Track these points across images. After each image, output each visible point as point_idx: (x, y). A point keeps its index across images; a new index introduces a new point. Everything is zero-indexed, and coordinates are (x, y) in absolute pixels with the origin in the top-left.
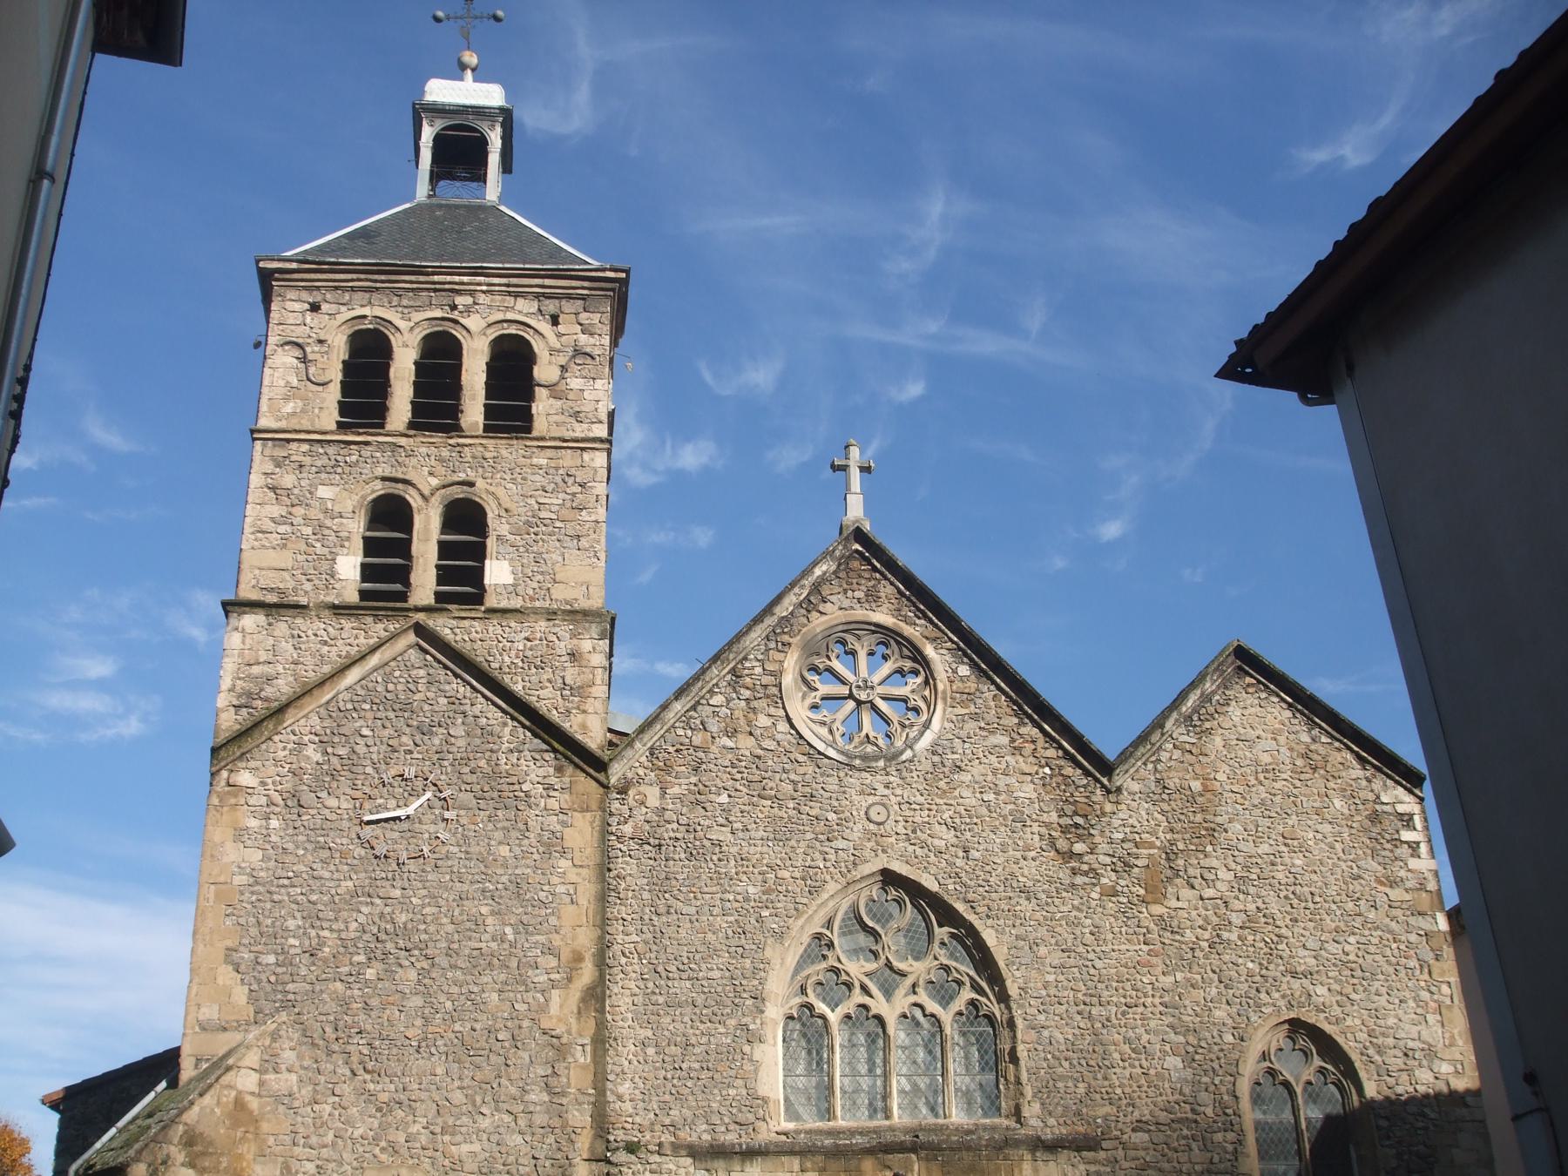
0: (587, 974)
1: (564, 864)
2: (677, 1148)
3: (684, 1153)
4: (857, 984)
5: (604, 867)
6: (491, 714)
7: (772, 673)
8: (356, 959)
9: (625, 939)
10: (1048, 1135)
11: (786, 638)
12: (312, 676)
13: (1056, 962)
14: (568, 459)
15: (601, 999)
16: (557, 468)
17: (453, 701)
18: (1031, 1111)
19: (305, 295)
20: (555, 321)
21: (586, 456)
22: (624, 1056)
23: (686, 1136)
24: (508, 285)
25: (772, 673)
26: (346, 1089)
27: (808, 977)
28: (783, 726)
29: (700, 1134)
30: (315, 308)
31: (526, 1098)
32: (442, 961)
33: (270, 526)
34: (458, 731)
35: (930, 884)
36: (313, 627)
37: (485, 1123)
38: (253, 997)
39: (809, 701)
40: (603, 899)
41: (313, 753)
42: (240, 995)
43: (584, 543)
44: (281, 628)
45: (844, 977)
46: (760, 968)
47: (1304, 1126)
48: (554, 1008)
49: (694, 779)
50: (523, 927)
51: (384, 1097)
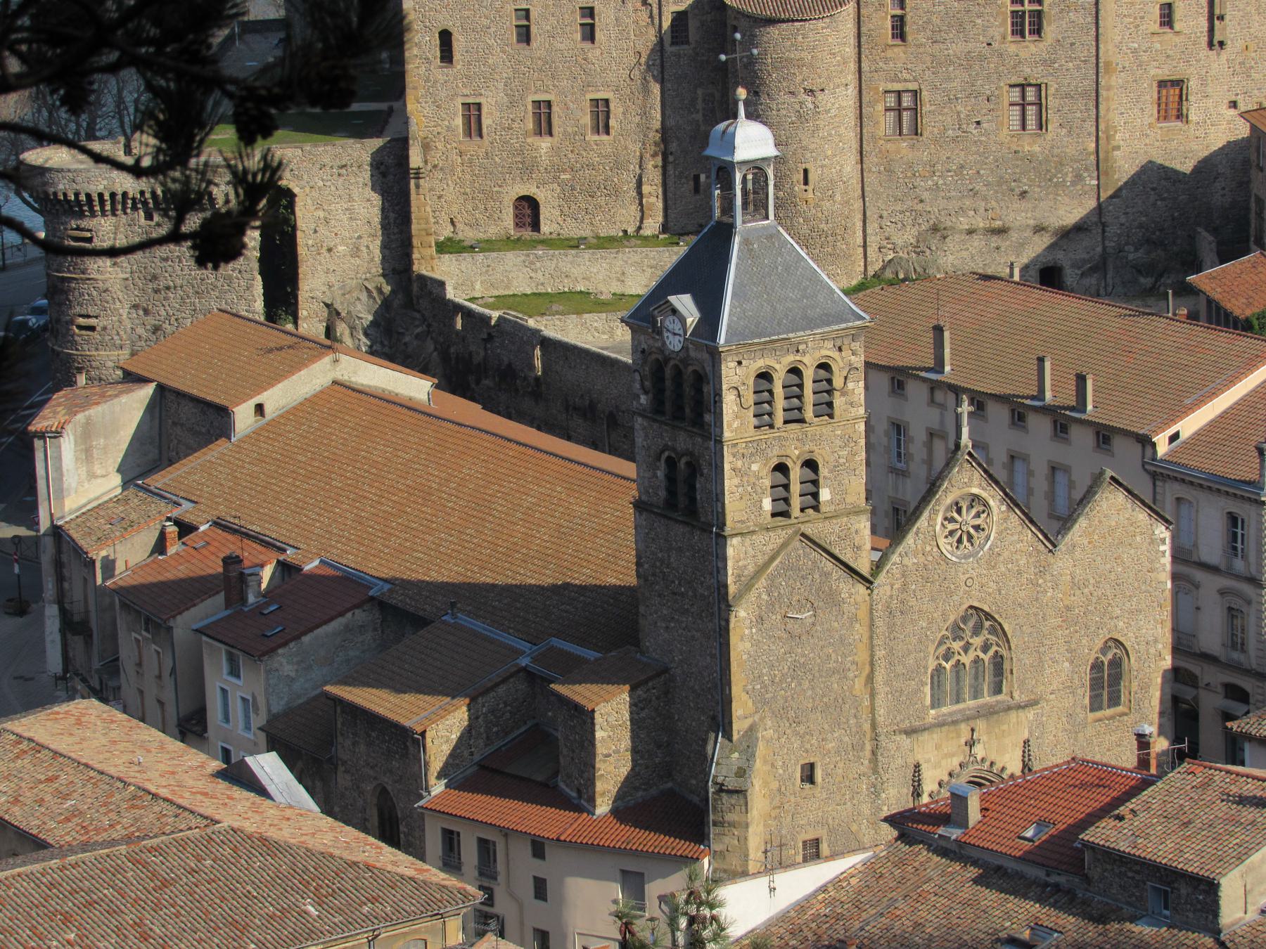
1: (858, 626)
2: (900, 732)
6: (829, 565)
12: (761, 562)
17: (814, 562)
18: (1016, 695)
20: (840, 349)
23: (902, 726)
26: (788, 731)
28: (935, 549)
29: (906, 725)
32: (817, 675)
34: (816, 576)
35: (986, 608)
36: (759, 538)
37: (836, 735)
38: (754, 702)
40: (871, 638)
41: (765, 597)
42: (750, 703)
47: (1039, 873)
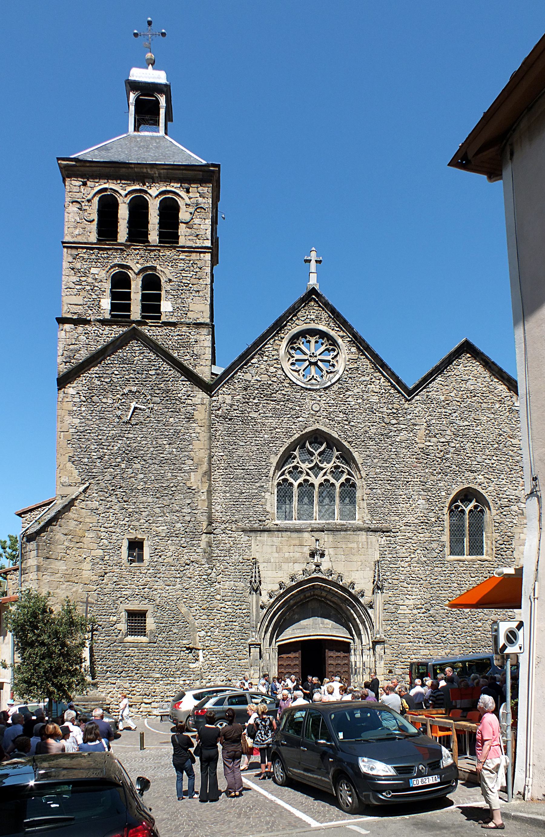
0: (205, 467)
5: (211, 426)
8: (117, 460)
10: (372, 526)
11: (282, 335)
22: (218, 497)
31: (182, 511)
39: (291, 361)
43: (201, 294)
44: (80, 329)
51: (130, 510)
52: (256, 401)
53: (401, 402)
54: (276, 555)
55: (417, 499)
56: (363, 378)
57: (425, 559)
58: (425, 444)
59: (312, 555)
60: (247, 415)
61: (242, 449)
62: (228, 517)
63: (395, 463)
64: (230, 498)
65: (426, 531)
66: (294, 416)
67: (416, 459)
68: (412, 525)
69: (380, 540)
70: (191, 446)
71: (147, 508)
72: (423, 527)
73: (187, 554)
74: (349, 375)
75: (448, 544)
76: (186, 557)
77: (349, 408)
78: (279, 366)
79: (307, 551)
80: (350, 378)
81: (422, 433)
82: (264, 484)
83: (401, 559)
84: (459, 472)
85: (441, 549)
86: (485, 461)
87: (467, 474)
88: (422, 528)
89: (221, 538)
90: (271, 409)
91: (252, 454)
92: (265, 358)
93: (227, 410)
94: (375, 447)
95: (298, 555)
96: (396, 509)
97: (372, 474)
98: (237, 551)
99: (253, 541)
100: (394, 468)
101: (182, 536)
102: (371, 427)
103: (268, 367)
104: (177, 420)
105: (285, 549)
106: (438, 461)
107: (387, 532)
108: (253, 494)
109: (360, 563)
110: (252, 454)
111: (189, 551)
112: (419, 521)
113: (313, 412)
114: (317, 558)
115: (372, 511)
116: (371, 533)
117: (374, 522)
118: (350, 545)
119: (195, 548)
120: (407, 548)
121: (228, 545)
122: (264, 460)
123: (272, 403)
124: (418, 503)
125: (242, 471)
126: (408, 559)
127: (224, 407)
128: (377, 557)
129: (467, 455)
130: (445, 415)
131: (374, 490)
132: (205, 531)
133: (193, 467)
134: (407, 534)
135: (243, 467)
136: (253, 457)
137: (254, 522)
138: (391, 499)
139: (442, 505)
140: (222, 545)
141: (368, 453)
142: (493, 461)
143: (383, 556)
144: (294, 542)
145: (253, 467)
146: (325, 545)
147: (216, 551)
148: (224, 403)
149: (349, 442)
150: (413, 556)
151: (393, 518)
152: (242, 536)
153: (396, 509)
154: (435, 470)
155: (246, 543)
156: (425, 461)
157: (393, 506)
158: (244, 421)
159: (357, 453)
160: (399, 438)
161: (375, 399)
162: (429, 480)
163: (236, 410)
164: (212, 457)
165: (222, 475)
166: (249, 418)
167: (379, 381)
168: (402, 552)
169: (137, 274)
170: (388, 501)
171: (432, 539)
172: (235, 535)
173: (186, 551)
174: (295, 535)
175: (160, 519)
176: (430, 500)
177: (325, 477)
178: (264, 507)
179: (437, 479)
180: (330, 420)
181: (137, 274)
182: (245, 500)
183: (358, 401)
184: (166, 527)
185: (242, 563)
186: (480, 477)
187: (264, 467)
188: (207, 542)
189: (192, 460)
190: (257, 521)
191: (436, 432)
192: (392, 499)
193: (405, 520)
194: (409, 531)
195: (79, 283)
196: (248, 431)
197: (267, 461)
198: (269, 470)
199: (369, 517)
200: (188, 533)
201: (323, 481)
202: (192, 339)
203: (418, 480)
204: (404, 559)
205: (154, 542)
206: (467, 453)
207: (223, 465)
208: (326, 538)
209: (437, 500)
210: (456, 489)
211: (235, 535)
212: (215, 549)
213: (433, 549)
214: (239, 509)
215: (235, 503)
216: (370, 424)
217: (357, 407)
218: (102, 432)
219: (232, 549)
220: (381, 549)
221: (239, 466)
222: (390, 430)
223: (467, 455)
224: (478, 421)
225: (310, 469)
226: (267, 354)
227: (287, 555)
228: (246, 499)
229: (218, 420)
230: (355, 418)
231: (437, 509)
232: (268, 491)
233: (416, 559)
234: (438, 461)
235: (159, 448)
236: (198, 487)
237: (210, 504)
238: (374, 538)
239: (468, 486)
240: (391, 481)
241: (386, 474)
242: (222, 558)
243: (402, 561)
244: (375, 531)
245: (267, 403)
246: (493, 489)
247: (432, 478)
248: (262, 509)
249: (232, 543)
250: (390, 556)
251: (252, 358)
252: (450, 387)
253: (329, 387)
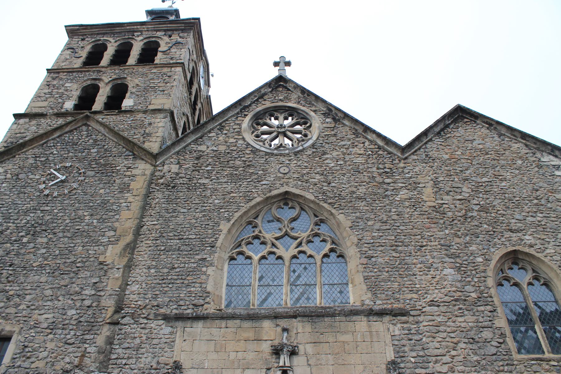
0: (129, 238)
3: (160, 318)
4: (269, 242)
5: (148, 195)
7: (238, 124)
9: (149, 222)
10: (376, 308)
11: (246, 113)
13: (378, 228)
14: (165, 70)
15: (134, 249)
16: (160, 73)
19: (80, 37)
21: (173, 69)
22: (139, 274)
24: (154, 28)
25: (238, 124)
27: (242, 240)
30: (83, 40)
33: (43, 95)
43: (166, 92)
44: (34, 122)
45: (262, 239)
46: (216, 233)
48: (108, 254)
49: (196, 162)
50: (102, 220)
51: (11, 293)
52: (209, 168)
53: (394, 162)
54: (214, 356)
55: (440, 268)
56: (343, 143)
57: (475, 358)
58: (437, 202)
59: (277, 352)
60: (196, 181)
61: (182, 217)
62: (147, 301)
63: (398, 224)
64: (155, 274)
65: (466, 313)
66: (256, 180)
67: (428, 219)
68: (442, 304)
69: (387, 330)
70: (117, 217)
71: (35, 290)
72: (461, 306)
73: (71, 355)
74: (325, 141)
75: (507, 330)
76: (67, 360)
77: (328, 169)
78: (241, 137)
79: (266, 347)
80: (326, 143)
81: (428, 191)
82: (208, 256)
83: (434, 359)
84: (494, 232)
85: (501, 341)
86: (527, 218)
87: (507, 234)
88: (460, 309)
89: (129, 330)
90: (226, 175)
91: (195, 221)
92: (225, 132)
93: (171, 178)
94: (367, 208)
95: (250, 356)
96: (411, 283)
97: (368, 239)
98: (151, 350)
99: (178, 334)
100: (399, 231)
101: (71, 327)
102: (359, 187)
103: (227, 139)
104: (108, 191)
105: (231, 346)
106: (459, 221)
107: (403, 315)
108: (189, 270)
109: (361, 367)
110: (195, 221)
111: (76, 349)
112: (452, 298)
113: (281, 175)
114: (284, 360)
115: (373, 287)
116: (375, 318)
117: (379, 302)
118: (342, 338)
119: (87, 346)
120: (440, 339)
121: (138, 341)
122: (212, 227)
123: (229, 169)
124: (444, 273)
125: (178, 241)
126: (447, 359)
127: (168, 176)
128: (390, 355)
129: (499, 212)
130: (455, 173)
131: (373, 259)
132: (108, 321)
133: (113, 239)
134: (435, 317)
135: (180, 237)
136: (196, 225)
137: (185, 307)
138: (401, 268)
139: (483, 274)
140: (128, 341)
141: (358, 214)
142: (539, 219)
143: (402, 354)
144: (245, 335)
145: (194, 237)
146: (299, 338)
147: (117, 351)
148: (170, 171)
149: (329, 204)
150: (453, 353)
151: (410, 296)
152: (163, 326)
153: (411, 283)
154: (459, 231)
155: (167, 336)
156: (442, 221)
157: (405, 279)
158: (191, 188)
159: (342, 215)
160: (399, 196)
161: (360, 160)
162: (453, 244)
163: (183, 177)
164: (142, 227)
165: (150, 246)
166: (198, 185)
167: (362, 145)
168: (433, 346)
169: (107, 84)
170: (397, 273)
171: (480, 324)
172: (152, 325)
173: (71, 350)
174: (247, 324)
175: (49, 303)
176: (462, 269)
177: (300, 249)
178: (204, 286)
179: (465, 241)
180: (302, 181)
181: (107, 84)
182: (176, 277)
183: (339, 163)
184: (52, 315)
185: (156, 369)
186: (527, 237)
187: (210, 236)
188: (108, 336)
189: (115, 231)
190: (191, 306)
191: (448, 189)
192: (403, 270)
193: (429, 298)
194: (438, 313)
195: (50, 93)
196: (194, 197)
197: (215, 228)
198: (217, 239)
199: (369, 295)
200: (82, 324)
201: (296, 253)
202: (147, 122)
203: (437, 243)
204: (439, 358)
205: (27, 336)
206: (498, 210)
207: (153, 235)
208: (301, 330)
209: (473, 269)
210: (497, 254)
211: (152, 325)
212: (118, 347)
213: (486, 341)
214: (166, 289)
215: (160, 282)
216: (356, 184)
217: (338, 168)
218: (15, 206)
219: (143, 346)
220: (396, 343)
221: (175, 235)
222: (384, 189)
223: (499, 212)
224: (501, 177)
225: (277, 239)
226: (227, 128)
227: (233, 355)
228: (178, 276)
229: (157, 188)
230: (337, 179)
231: (476, 280)
232: (211, 265)
233: (460, 358)
234: (459, 221)
235: (78, 220)
236: (113, 263)
237: (125, 285)
238: (381, 326)
239: (514, 248)
240: (396, 246)
241: (388, 238)
242: (124, 362)
243: (436, 362)
244: (381, 314)
245: (222, 170)
246: (553, 251)
247: (457, 240)
248: (200, 289)
249: (144, 338)
250: (414, 354)
251: (210, 132)
252: (453, 147)
253: (301, 151)
